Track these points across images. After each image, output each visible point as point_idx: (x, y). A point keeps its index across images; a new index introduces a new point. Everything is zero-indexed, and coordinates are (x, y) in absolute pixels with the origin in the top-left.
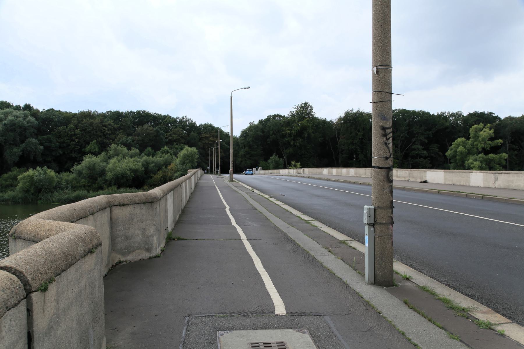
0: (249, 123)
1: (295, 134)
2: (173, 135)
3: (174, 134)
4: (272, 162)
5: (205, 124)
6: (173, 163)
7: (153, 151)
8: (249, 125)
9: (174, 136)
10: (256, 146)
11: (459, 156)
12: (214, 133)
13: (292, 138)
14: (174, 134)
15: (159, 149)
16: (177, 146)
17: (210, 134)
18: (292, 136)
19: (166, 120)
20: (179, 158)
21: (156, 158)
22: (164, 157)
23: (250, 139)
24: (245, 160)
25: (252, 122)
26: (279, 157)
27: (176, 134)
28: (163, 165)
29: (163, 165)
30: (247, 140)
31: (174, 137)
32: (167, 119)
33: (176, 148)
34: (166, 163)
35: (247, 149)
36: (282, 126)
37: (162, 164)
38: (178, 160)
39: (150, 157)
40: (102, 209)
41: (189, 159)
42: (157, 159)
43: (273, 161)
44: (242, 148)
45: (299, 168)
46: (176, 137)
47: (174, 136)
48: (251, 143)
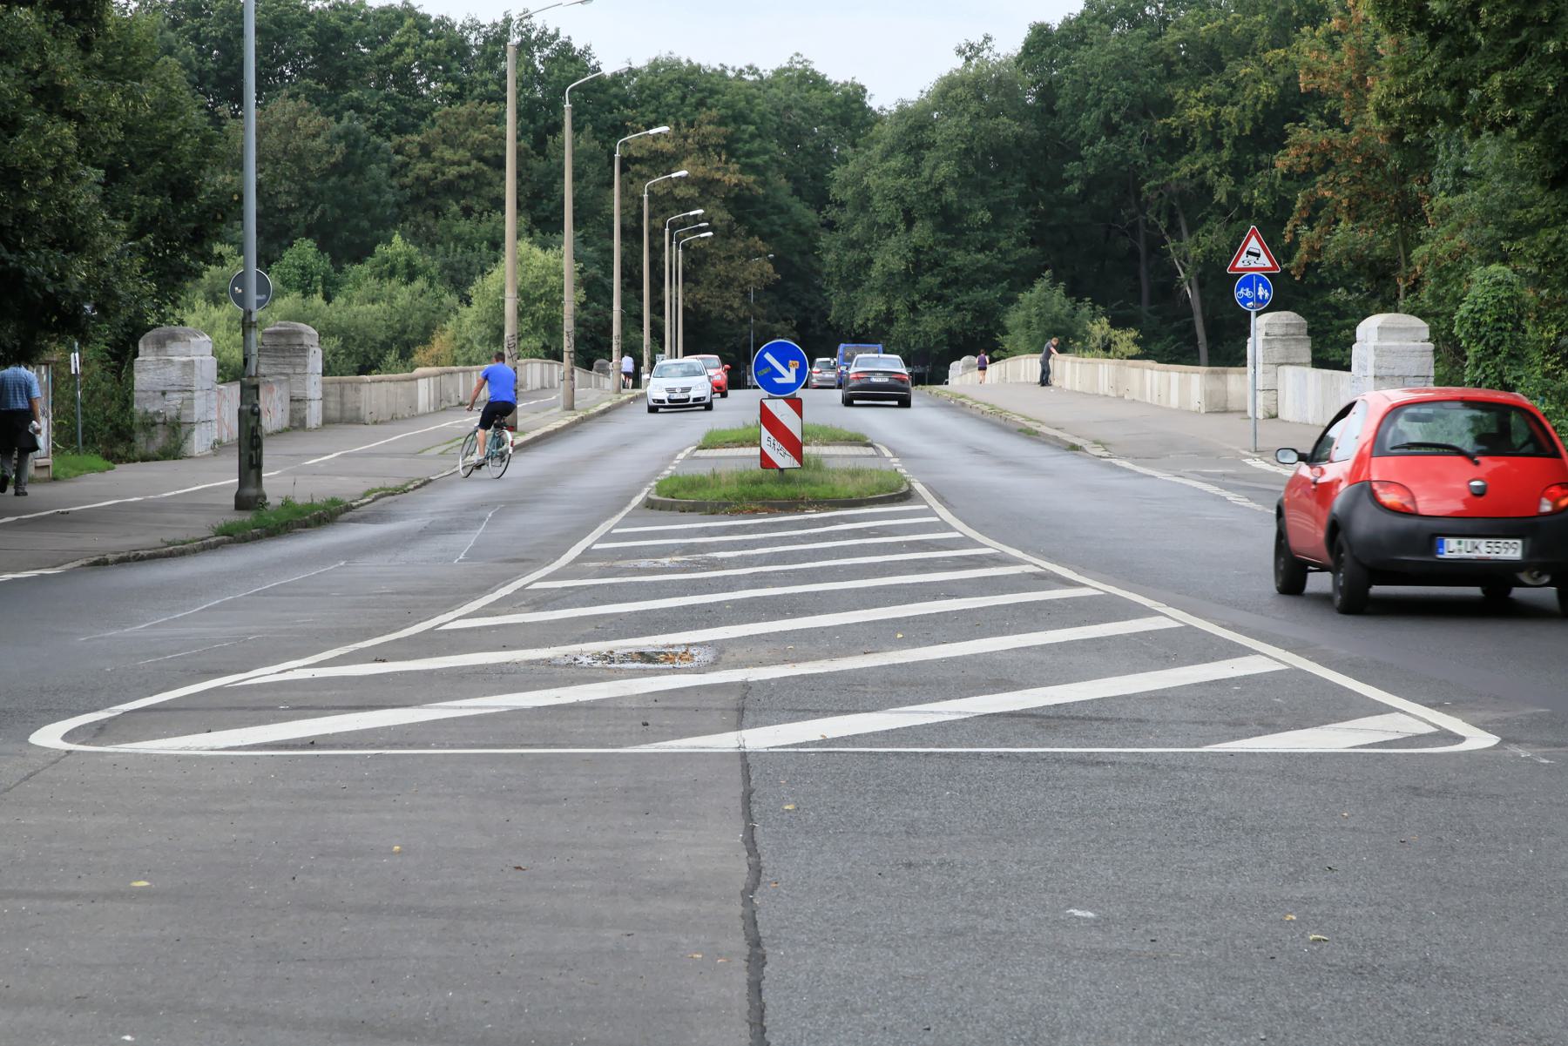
0: (960, 52)
1: (1242, 129)
2: (442, 147)
3: (444, 142)
4: (1028, 325)
5: (655, 66)
6: (443, 330)
7: (324, 264)
8: (959, 62)
9: (448, 154)
10: (987, 216)
11: (1084, 315)
12: (710, 128)
13: (1225, 155)
14: (449, 140)
15: (360, 253)
16: (464, 226)
17: (686, 137)
18: (1225, 141)
19: (397, 45)
20: (475, 307)
21: (350, 301)
22: (392, 298)
23: (945, 169)
24: (913, 308)
25: (977, 39)
26: (1069, 293)
27: (463, 145)
28: (386, 346)
29: (386, 346)
30: (926, 173)
31: (443, 162)
32: (404, 39)
33: (458, 239)
34: (404, 331)
35: (922, 232)
36: (1171, 75)
37: (381, 337)
38: (472, 317)
39: (318, 300)
40: (436, 376)
41: (532, 315)
42: (355, 308)
43: (1034, 320)
44: (891, 226)
45: (1129, 358)
46: (459, 163)
47: (448, 154)
48: (950, 194)
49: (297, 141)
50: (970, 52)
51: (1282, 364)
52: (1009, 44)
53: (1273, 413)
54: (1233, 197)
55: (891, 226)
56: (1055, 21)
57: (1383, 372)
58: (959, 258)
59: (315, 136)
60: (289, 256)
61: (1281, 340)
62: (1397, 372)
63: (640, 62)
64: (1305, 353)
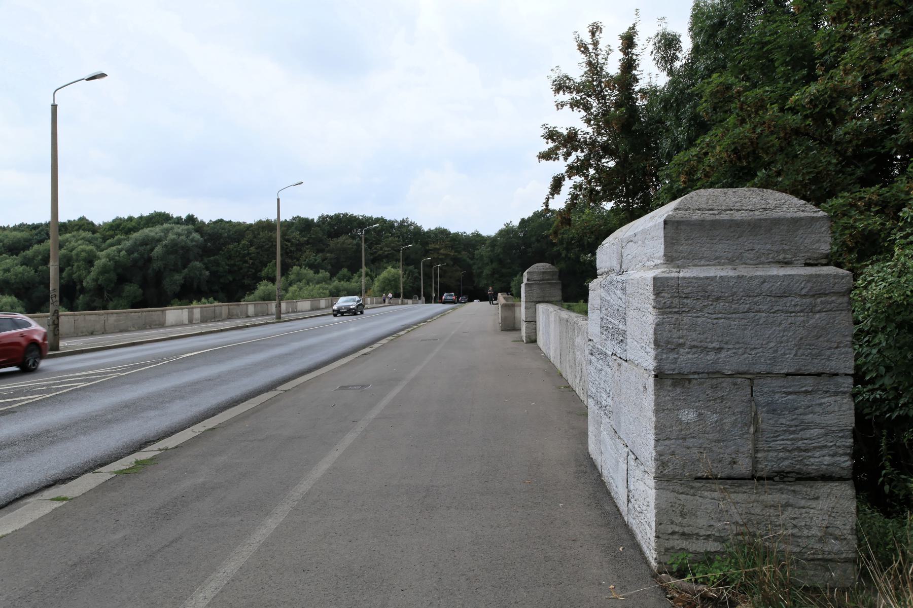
7: (349, 274)
8: (504, 227)
9: (386, 249)
14: (387, 246)
24: (493, 282)
35: (495, 265)
44: (487, 264)
47: (386, 249)
48: (501, 256)
49: (345, 245)
50: (507, 225)
51: (539, 302)
52: (516, 223)
53: (533, 338)
54: (566, 256)
55: (487, 264)
56: (526, 218)
57: (686, 360)
58: (504, 270)
59: (349, 244)
60: (341, 272)
61: (538, 284)
62: (729, 361)
63: (433, 228)
64: (557, 294)
